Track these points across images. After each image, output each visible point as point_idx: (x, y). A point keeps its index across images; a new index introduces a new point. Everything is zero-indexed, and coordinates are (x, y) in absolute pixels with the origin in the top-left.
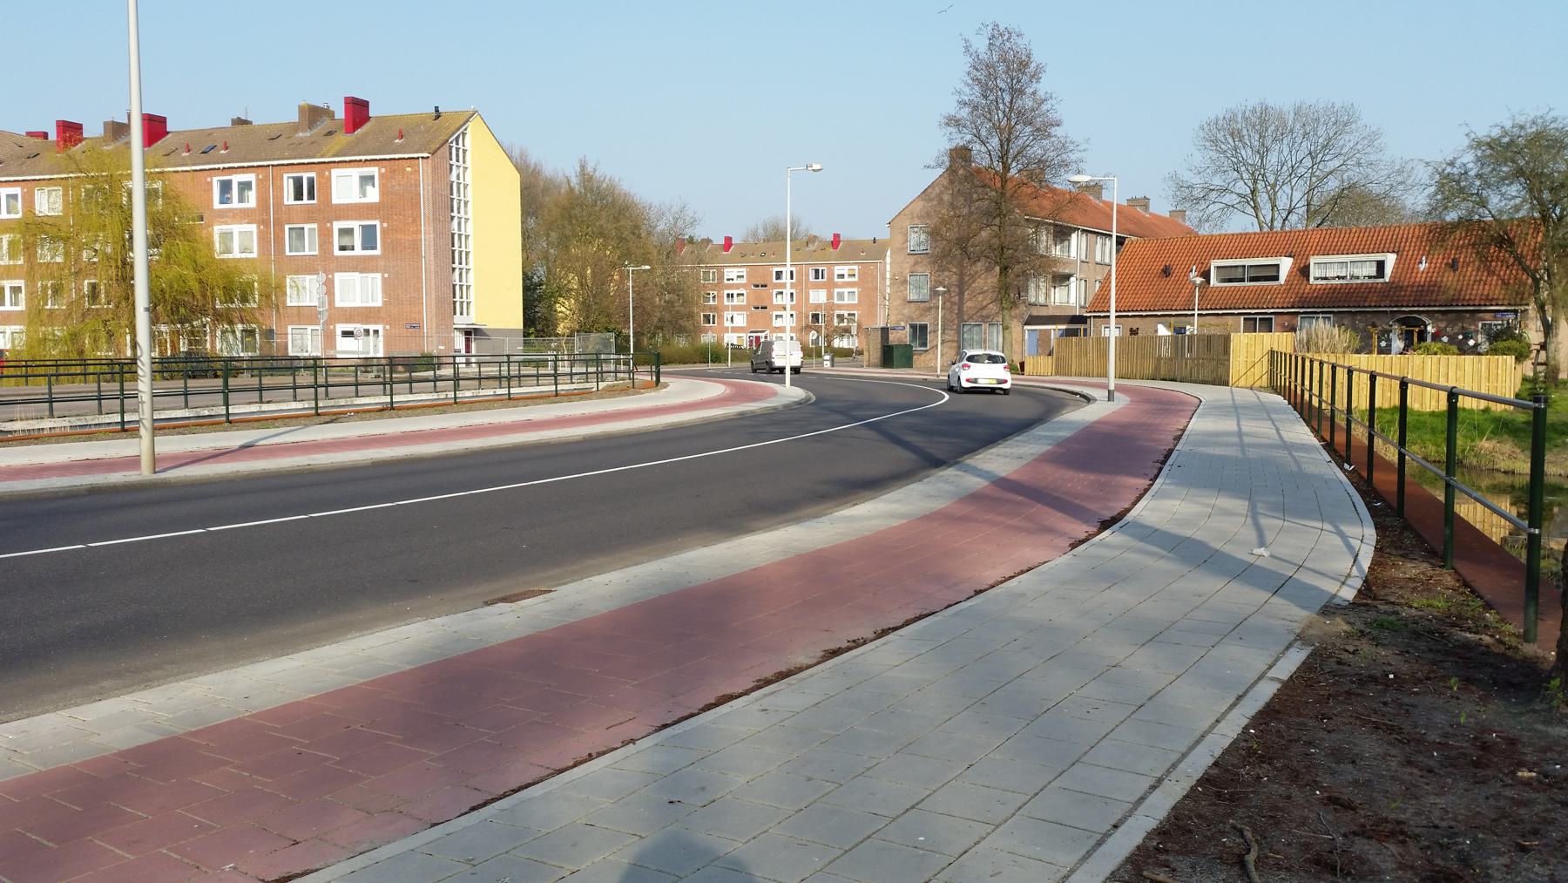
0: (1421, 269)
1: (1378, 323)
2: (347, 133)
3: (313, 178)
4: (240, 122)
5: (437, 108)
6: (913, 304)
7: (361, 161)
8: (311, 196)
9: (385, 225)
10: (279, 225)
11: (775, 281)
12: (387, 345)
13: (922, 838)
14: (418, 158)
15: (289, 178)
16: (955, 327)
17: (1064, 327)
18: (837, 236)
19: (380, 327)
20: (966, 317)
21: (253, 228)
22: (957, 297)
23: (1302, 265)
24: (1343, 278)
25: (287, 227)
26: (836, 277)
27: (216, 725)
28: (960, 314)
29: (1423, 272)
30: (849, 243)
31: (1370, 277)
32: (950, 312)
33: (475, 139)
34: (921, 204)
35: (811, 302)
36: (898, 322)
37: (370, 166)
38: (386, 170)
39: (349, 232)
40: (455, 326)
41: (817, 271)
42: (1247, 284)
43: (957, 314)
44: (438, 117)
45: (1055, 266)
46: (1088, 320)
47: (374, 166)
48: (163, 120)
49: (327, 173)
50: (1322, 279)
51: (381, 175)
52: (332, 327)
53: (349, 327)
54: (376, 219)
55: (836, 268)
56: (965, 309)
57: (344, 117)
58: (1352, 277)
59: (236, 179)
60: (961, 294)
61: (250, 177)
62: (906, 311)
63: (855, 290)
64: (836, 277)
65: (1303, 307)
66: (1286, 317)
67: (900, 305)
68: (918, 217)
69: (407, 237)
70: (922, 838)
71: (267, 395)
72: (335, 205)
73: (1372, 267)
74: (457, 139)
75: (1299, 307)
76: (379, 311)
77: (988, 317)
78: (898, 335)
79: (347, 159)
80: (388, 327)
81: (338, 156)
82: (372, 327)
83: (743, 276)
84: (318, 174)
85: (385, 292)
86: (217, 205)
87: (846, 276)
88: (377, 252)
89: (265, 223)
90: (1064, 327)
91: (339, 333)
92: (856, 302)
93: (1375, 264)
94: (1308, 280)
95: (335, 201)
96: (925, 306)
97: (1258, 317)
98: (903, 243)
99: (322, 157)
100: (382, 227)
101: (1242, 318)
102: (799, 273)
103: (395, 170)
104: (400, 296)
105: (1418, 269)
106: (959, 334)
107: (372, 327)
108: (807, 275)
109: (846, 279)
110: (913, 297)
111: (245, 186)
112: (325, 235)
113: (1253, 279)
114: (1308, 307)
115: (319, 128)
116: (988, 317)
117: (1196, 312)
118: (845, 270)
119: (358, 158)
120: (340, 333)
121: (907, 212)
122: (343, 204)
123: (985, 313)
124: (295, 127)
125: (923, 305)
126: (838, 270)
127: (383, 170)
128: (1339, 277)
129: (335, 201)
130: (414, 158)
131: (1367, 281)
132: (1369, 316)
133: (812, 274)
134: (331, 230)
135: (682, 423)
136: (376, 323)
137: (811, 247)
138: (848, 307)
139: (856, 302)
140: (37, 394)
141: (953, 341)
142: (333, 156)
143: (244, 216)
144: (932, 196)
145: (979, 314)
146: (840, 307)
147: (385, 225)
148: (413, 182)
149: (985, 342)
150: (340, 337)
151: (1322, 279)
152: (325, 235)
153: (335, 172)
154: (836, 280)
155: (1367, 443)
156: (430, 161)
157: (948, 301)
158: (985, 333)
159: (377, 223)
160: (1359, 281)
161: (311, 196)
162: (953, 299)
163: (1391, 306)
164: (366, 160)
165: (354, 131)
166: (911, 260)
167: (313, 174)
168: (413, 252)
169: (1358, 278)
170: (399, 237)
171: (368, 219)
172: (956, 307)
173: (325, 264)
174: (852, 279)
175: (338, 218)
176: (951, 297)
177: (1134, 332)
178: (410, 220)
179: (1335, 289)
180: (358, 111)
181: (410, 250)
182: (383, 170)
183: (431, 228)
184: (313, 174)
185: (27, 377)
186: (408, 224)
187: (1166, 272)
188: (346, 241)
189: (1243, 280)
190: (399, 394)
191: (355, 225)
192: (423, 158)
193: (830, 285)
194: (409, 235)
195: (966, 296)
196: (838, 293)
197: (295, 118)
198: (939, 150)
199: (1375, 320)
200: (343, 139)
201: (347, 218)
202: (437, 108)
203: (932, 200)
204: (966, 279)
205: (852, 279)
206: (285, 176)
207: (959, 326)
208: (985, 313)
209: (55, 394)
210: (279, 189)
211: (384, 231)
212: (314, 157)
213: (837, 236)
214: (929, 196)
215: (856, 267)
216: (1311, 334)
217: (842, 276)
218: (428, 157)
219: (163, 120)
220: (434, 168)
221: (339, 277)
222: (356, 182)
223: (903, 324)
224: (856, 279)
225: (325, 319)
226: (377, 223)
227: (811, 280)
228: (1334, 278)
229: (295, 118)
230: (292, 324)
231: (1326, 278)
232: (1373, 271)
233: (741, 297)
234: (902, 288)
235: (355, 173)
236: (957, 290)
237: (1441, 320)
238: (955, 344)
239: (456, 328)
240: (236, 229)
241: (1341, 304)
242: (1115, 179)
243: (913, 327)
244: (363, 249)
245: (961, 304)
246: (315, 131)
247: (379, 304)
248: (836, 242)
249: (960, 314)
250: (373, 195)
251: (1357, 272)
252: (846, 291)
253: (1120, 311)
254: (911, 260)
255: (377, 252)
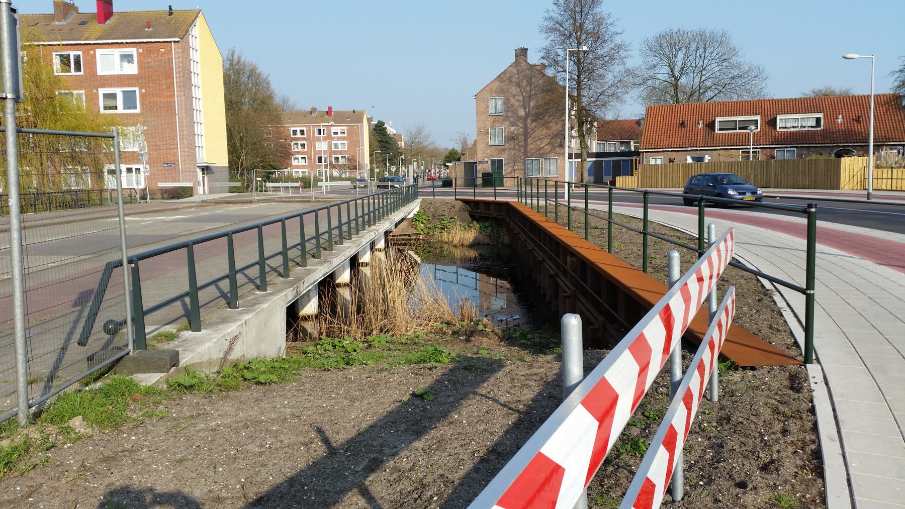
0: (839, 122)
1: (823, 152)
2: (99, 23)
3: (79, 56)
6: (493, 147)
7: (122, 43)
8: (78, 68)
9: (143, 91)
14: (171, 42)
15: (56, 55)
16: (522, 161)
17: (594, 159)
18: (330, 108)
20: (529, 155)
22: (523, 142)
23: (767, 120)
24: (796, 127)
26: (332, 134)
28: (525, 153)
29: (841, 124)
30: (337, 113)
31: (812, 127)
32: (519, 152)
33: (199, 34)
34: (497, 84)
35: (317, 149)
37: (130, 47)
38: (143, 51)
39: (113, 96)
40: (198, 165)
41: (320, 130)
42: (738, 131)
43: (523, 153)
44: (171, 14)
46: (641, 154)
47: (133, 47)
49: (92, 52)
50: (783, 128)
51: (139, 55)
54: (135, 86)
55: (332, 128)
56: (529, 150)
57: (96, 11)
58: (802, 127)
60: (526, 140)
63: (345, 142)
64: (332, 134)
65: (779, 144)
66: (768, 150)
67: (484, 148)
68: (495, 92)
69: (162, 100)
71: (804, 205)
72: (101, 76)
73: (813, 121)
75: (776, 144)
77: (544, 154)
78: (483, 167)
79: (110, 41)
81: (101, 39)
82: (134, 167)
83: (344, 133)
84: (84, 53)
87: (339, 133)
90: (594, 159)
91: (105, 170)
92: (346, 149)
93: (815, 120)
94: (775, 129)
95: (100, 72)
96: (501, 149)
97: (786, 149)
98: (485, 109)
99: (86, 39)
100: (141, 93)
101: (741, 151)
102: (309, 131)
103: (150, 51)
104: (158, 143)
105: (837, 122)
106: (525, 166)
107: (134, 167)
108: (314, 132)
109: (339, 135)
110: (491, 142)
113: (740, 128)
114: (782, 144)
115: (70, 18)
116: (544, 154)
117: (752, 147)
118: (338, 129)
119: (120, 41)
120: (125, 170)
121: (487, 88)
122: (107, 76)
123: (541, 152)
124: (51, 18)
125: (500, 147)
126: (334, 130)
127: (141, 50)
128: (793, 127)
129: (100, 72)
130: (167, 42)
131: (810, 129)
132: (818, 148)
133: (316, 132)
135: (769, 219)
136: (137, 163)
137: (314, 115)
138: (340, 152)
139: (346, 149)
141: (521, 169)
142: (97, 39)
144: (505, 79)
145: (538, 153)
146: (336, 153)
147: (143, 91)
148: (166, 59)
149: (542, 170)
150: (125, 172)
151: (783, 128)
154: (333, 135)
156: (180, 44)
157: (517, 144)
158: (542, 164)
160: (806, 129)
161: (78, 68)
162: (520, 143)
163: (831, 143)
164: (127, 43)
165: (105, 22)
166: (491, 119)
167: (80, 53)
168: (168, 110)
169: (805, 127)
170: (155, 100)
171: (129, 86)
172: (523, 149)
174: (343, 135)
175: (103, 86)
176: (519, 142)
177: (671, 161)
178: (164, 87)
179: (793, 133)
181: (165, 109)
182: (141, 50)
183: (182, 93)
184: (80, 53)
186: (163, 90)
187: (682, 124)
188: (110, 103)
189: (735, 129)
191: (119, 91)
192: (174, 42)
193: (329, 138)
194: (164, 98)
195: (530, 141)
196: (335, 144)
197: (50, 10)
198: (522, 53)
199: (821, 151)
200: (97, 28)
201: (111, 86)
203: (505, 81)
204: (529, 131)
205: (343, 135)
206: (54, 53)
207: (524, 160)
208: (541, 152)
209: (606, 204)
212: (80, 40)
213: (330, 108)
214: (502, 78)
215: (345, 128)
217: (336, 133)
218: (179, 41)
222: (117, 58)
223: (486, 159)
224: (346, 135)
226: (137, 89)
227: (316, 135)
228: (790, 128)
229: (50, 10)
231: (786, 128)
232: (814, 124)
234: (485, 137)
235: (117, 52)
236: (523, 138)
237: (860, 150)
238: (523, 171)
239: (198, 166)
241: (801, 142)
242: (873, 57)
243: (493, 162)
244: (124, 109)
245: (526, 146)
246: (68, 21)
248: (329, 113)
249: (525, 153)
250: (132, 69)
251: (804, 124)
252: (339, 142)
253: (877, 142)
254: (491, 119)
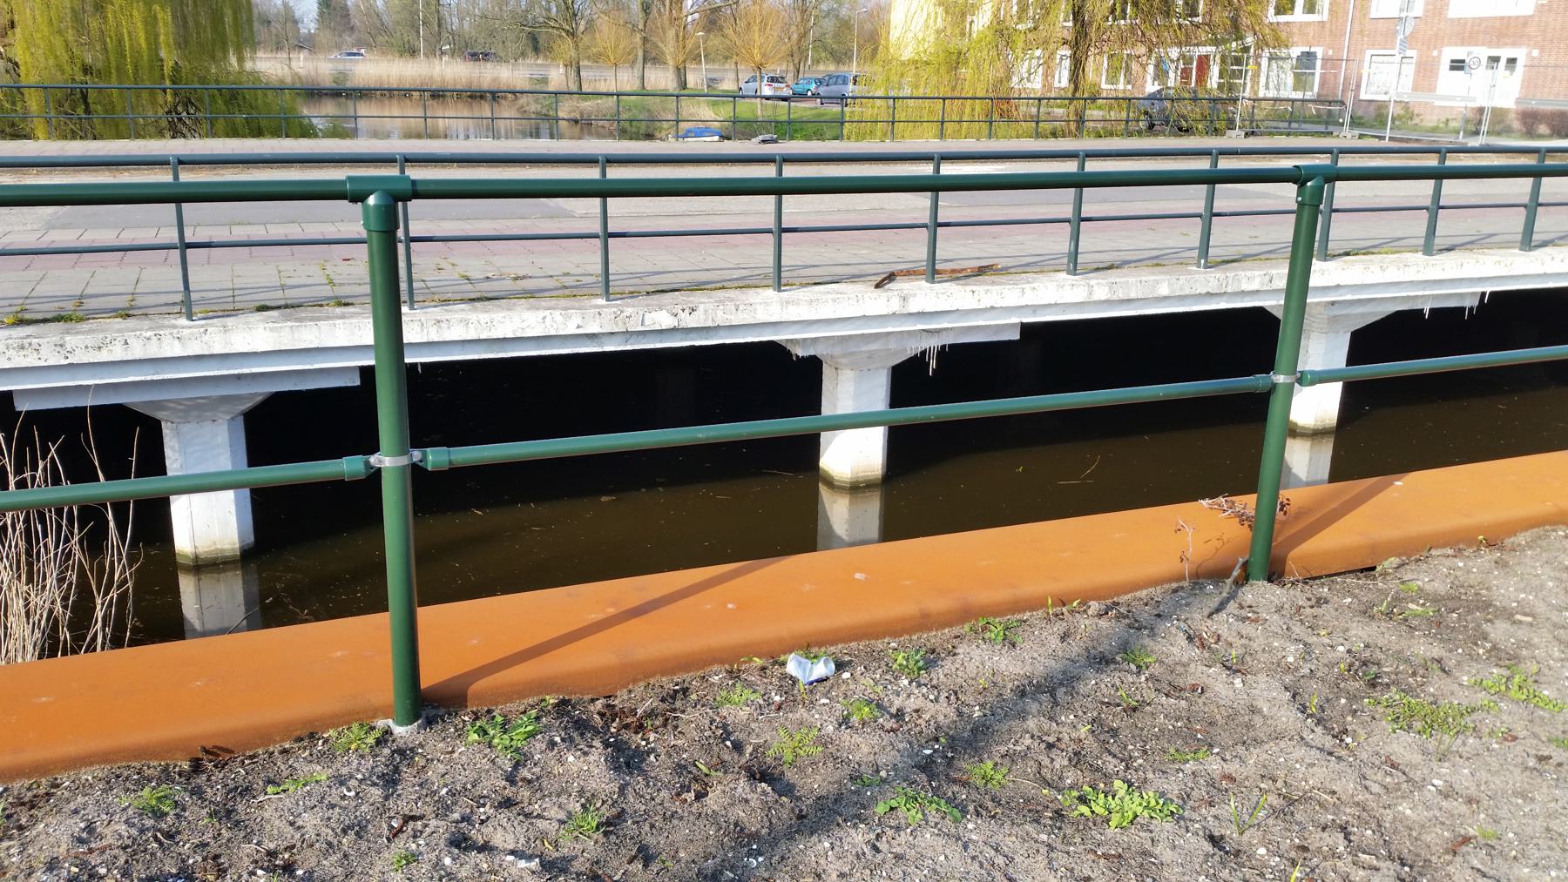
12: (1527, 83)
13: (858, 576)
19: (1520, 53)
27: (1353, 498)
45: (251, 50)
52: (1435, 53)
53: (1459, 53)
70: (858, 576)
76: (1525, 24)
80: (1536, 53)
82: (1505, 53)
136: (1514, 44)
140: (1408, 140)
185: (944, 99)
216: (122, 34)
225: (1407, 33)
230: (1373, 46)
233: (542, 40)
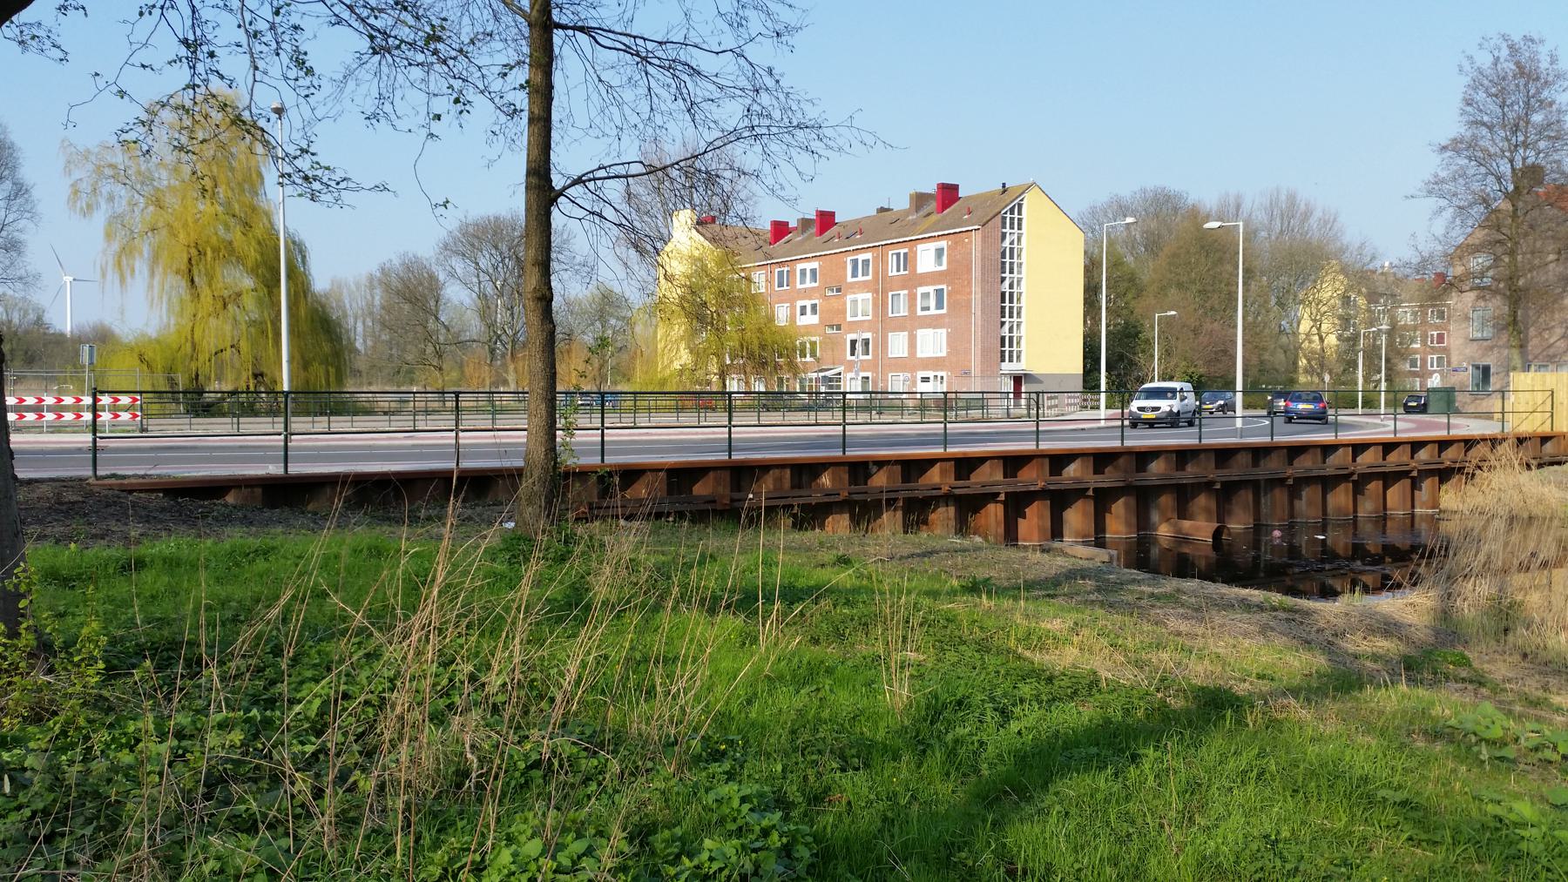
4: (882, 210)
5: (1004, 185)
10: (885, 293)
11: (849, 357)
19: (944, 374)
20: (1530, 357)
21: (869, 296)
25: (890, 294)
36: (1460, 363)
48: (955, 188)
59: (861, 257)
61: (868, 256)
62: (1467, 351)
74: (1012, 211)
77: (1555, 356)
82: (939, 374)
85: (949, 344)
86: (850, 279)
88: (944, 311)
89: (876, 291)
111: (866, 262)
112: (912, 298)
116: (1555, 356)
123: (1551, 351)
124: (907, 213)
125: (1485, 343)
134: (916, 295)
143: (864, 286)
152: (912, 298)
153: (920, 247)
155: (1121, 501)
159: (944, 287)
173: (911, 324)
180: (948, 194)
190: (79, 450)
191: (931, 289)
202: (1004, 185)
208: (1551, 351)
210: (885, 262)
211: (949, 294)
219: (955, 188)
220: (984, 238)
221: (920, 333)
222: (932, 254)
223: (1465, 365)
226: (944, 287)
235: (932, 246)
240: (860, 296)
247: (944, 354)
255: (944, 311)
